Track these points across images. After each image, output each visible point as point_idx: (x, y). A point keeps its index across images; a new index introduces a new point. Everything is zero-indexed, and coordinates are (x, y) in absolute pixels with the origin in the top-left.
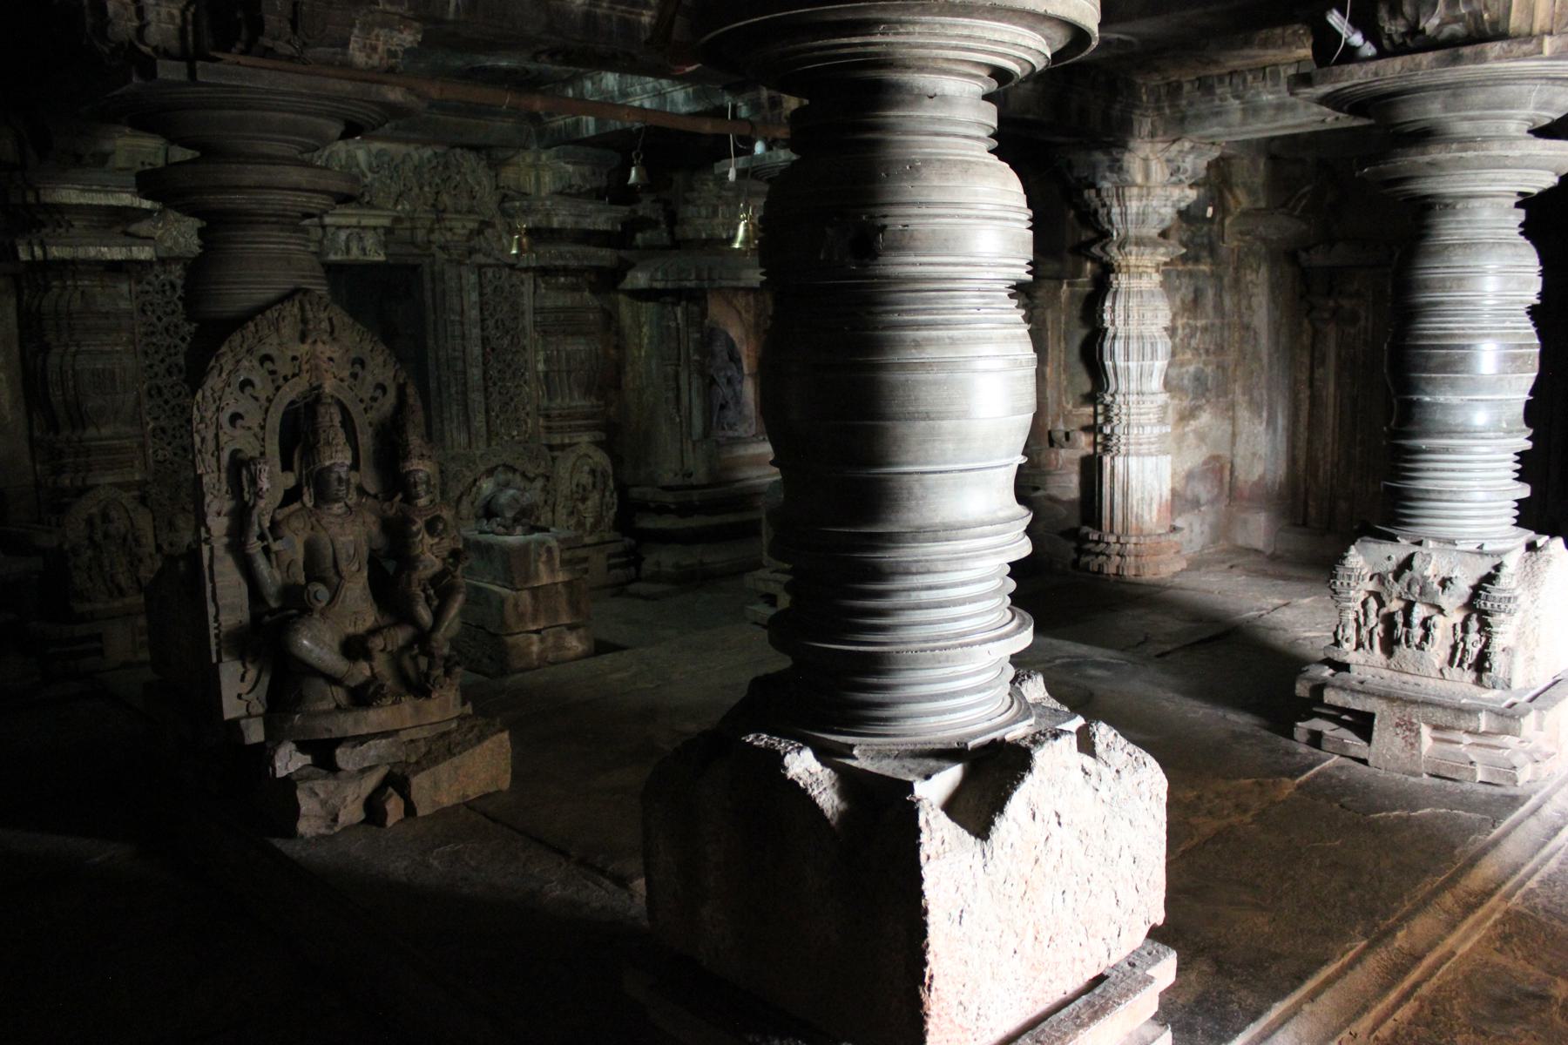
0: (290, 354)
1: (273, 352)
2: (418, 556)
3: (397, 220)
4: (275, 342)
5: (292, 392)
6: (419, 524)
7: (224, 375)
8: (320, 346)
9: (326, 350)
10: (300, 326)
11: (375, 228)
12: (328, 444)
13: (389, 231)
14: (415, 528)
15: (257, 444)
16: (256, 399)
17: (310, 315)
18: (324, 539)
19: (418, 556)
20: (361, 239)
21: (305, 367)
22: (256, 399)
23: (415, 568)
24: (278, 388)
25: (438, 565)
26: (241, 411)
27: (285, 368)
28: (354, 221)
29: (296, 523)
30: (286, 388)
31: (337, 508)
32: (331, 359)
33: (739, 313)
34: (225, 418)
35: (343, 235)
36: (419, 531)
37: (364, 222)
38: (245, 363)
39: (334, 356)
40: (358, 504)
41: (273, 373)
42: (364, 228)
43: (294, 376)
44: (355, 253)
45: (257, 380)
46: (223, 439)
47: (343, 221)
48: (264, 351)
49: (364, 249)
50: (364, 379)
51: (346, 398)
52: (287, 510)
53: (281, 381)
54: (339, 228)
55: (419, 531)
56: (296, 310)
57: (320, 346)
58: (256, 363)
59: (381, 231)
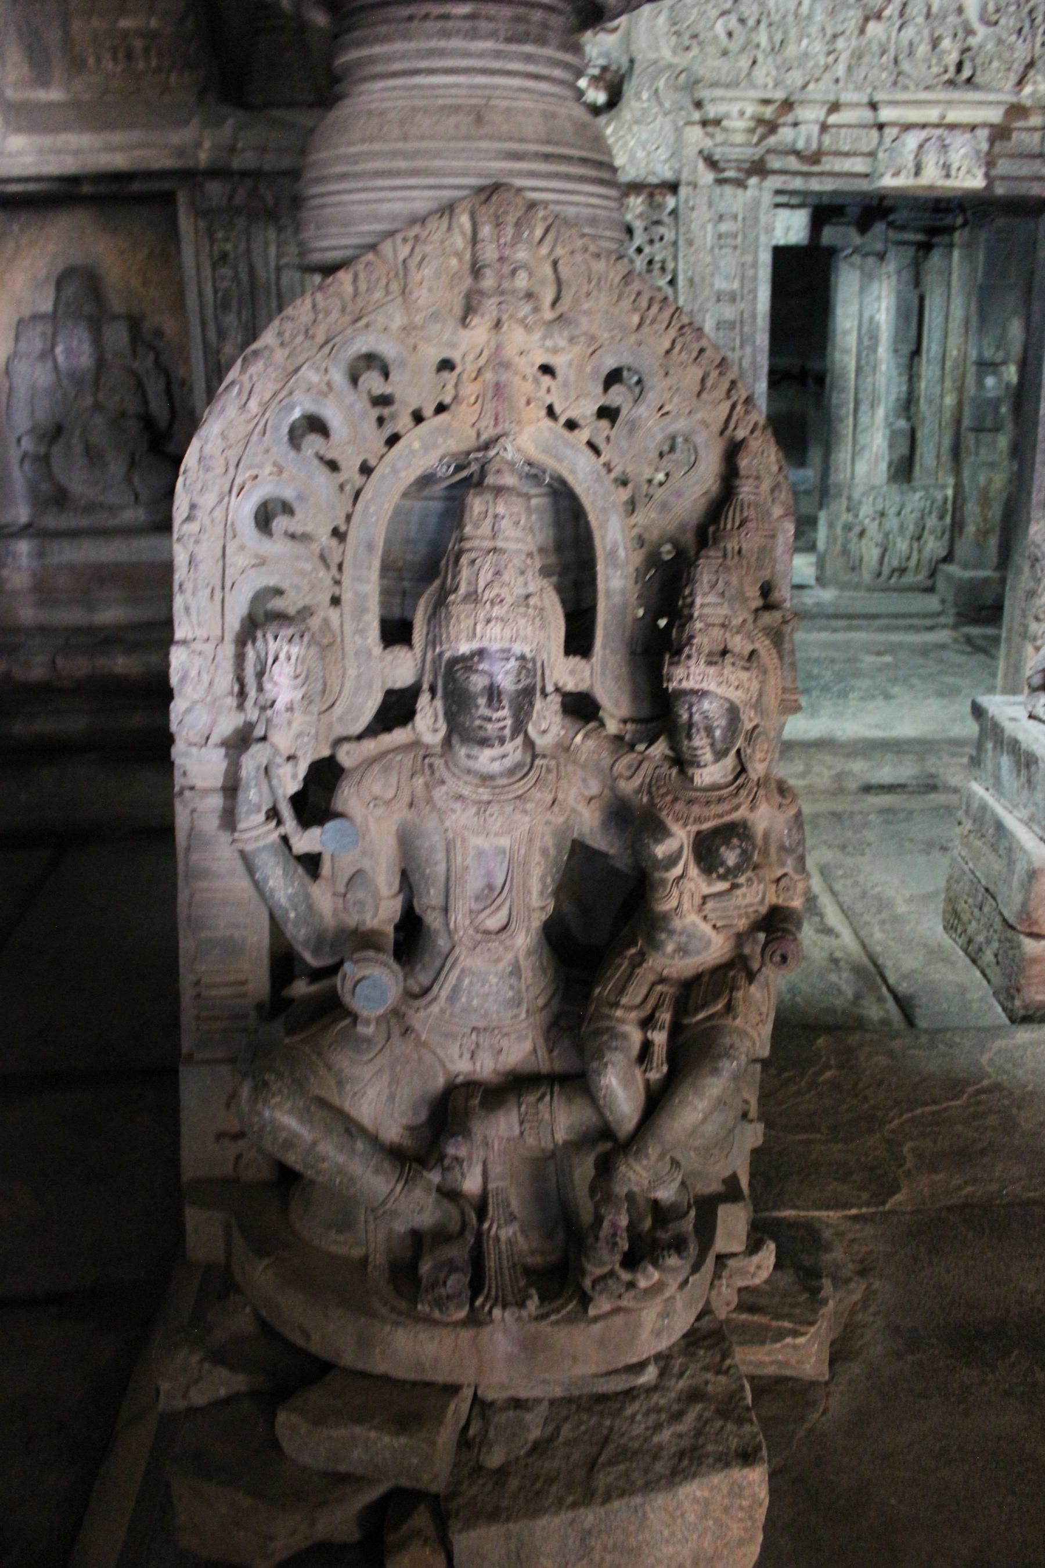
0: (433, 354)
1: (388, 349)
2: (665, 917)
3: (1017, 111)
4: (398, 321)
5: (424, 451)
6: (679, 838)
7: (253, 405)
8: (516, 337)
9: (526, 345)
10: (468, 282)
11: (973, 128)
12: (473, 597)
13: (1000, 133)
14: (661, 851)
15: (325, 577)
16: (333, 466)
17: (489, 253)
18: (432, 842)
19: (665, 917)
20: (944, 147)
21: (470, 390)
22: (333, 466)
23: (655, 945)
24: (393, 440)
25: (715, 948)
26: (288, 494)
27: (413, 388)
28: (932, 115)
29: (376, 784)
30: (413, 439)
31: (486, 759)
32: (547, 369)
33: (459, 375)
34: (245, 509)
35: (912, 140)
36: (672, 860)
37: (952, 117)
38: (310, 375)
39: (558, 361)
40: (565, 748)
41: (383, 401)
42: (952, 127)
43: (441, 408)
44: (931, 176)
45: (332, 414)
46: (238, 561)
47: (913, 115)
48: (363, 344)
49: (946, 167)
50: (633, 427)
51: (581, 472)
52: (370, 746)
53: (404, 421)
54: (907, 127)
55: (672, 860)
56: (459, 242)
57: (516, 337)
58: (339, 377)
59: (983, 134)
